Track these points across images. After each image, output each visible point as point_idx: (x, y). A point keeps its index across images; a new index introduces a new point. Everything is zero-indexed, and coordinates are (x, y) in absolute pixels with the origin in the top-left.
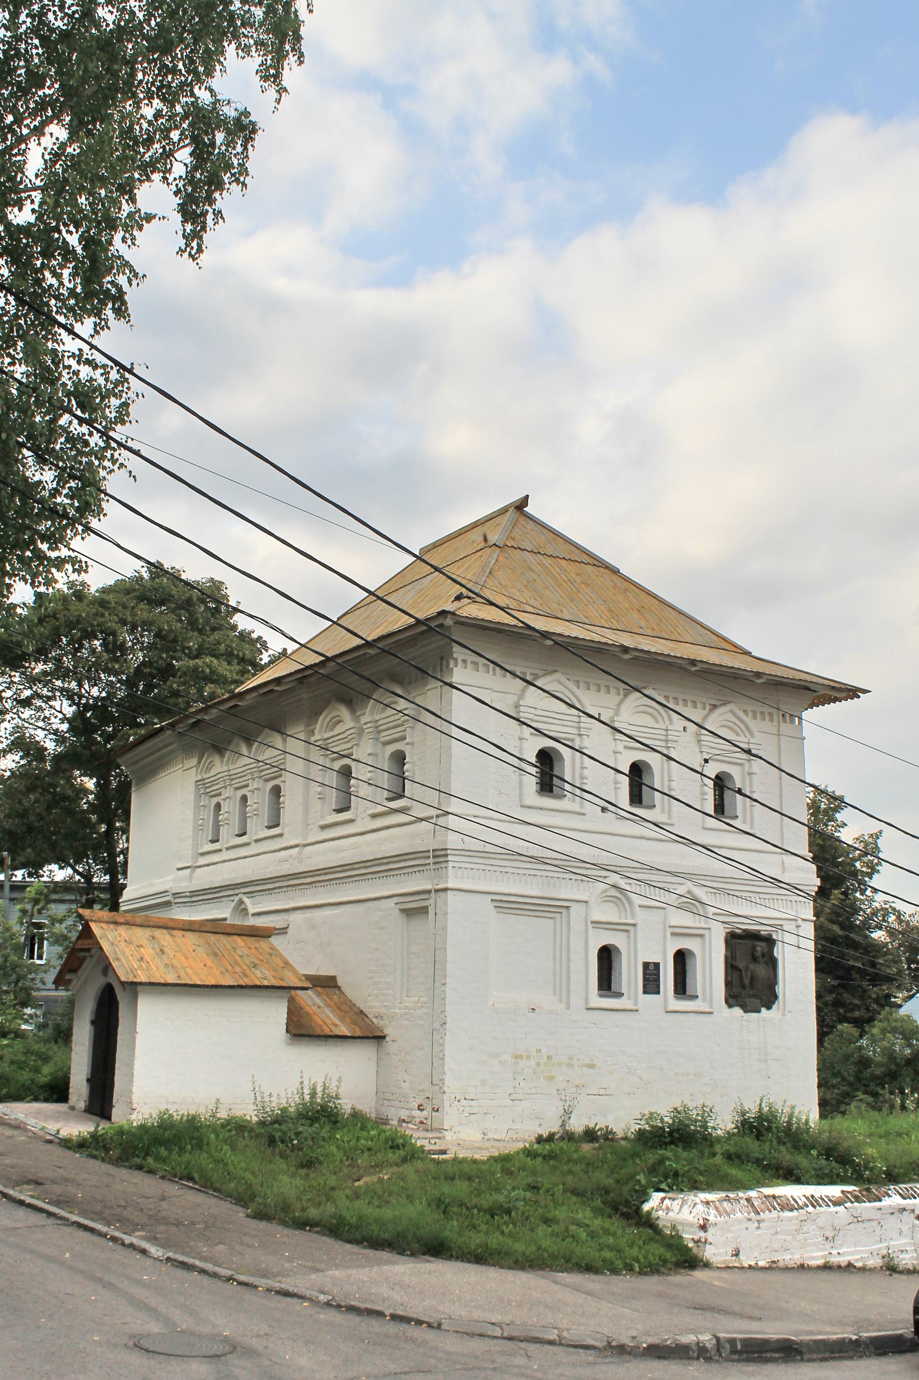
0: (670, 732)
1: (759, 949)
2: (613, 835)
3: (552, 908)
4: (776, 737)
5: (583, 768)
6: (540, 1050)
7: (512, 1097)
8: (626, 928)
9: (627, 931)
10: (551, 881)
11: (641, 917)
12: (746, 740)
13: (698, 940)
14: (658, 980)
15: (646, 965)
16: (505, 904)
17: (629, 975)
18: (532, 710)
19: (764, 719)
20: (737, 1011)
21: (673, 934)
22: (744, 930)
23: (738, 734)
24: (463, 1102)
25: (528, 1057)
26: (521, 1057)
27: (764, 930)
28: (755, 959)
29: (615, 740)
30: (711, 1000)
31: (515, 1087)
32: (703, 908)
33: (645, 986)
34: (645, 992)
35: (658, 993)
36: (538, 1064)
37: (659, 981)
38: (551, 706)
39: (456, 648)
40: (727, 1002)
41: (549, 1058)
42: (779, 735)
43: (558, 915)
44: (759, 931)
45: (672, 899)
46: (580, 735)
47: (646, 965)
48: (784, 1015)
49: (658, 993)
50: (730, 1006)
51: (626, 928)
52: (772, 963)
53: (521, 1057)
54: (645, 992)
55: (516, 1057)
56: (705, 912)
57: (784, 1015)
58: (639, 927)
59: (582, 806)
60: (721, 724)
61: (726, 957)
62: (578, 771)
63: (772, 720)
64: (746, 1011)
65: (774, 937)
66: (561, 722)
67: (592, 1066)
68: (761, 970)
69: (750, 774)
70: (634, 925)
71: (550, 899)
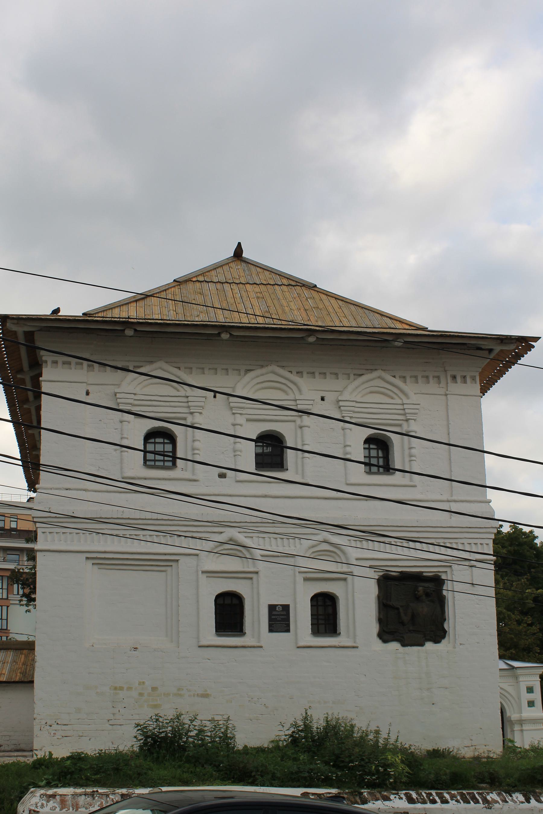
0: (190, 399)
1: (420, 589)
2: (245, 496)
3: (165, 563)
4: (444, 398)
5: (410, 448)
6: (144, 683)
7: (111, 722)
8: (248, 576)
9: (251, 579)
10: (63, 537)
11: (261, 566)
12: (400, 402)
13: (341, 583)
14: (288, 619)
15: (272, 608)
16: (101, 561)
17: (255, 616)
18: (132, 396)
19: (465, 382)
20: (395, 646)
21: (306, 579)
22: (401, 572)
23: (392, 398)
24: (55, 727)
25: (130, 689)
26: (121, 688)
27: (428, 571)
28: (417, 598)
29: (234, 414)
30: (355, 636)
31: (114, 714)
32: (248, 551)
33: (270, 626)
34: (271, 630)
35: (288, 631)
36: (141, 694)
37: (289, 621)
38: (151, 392)
39: (42, 353)
40: (444, 637)
41: (154, 689)
42: (446, 395)
43: (169, 569)
44: (423, 572)
45: (208, 546)
46: (192, 413)
47: (272, 608)
48: (454, 647)
49: (288, 631)
50: (385, 641)
51: (248, 576)
52: (441, 601)
53: (121, 688)
54: (271, 630)
55: (116, 688)
56: (251, 554)
57: (454, 647)
58: (261, 574)
59: (411, 480)
60: (368, 390)
61: (379, 597)
62: (407, 452)
63: (439, 383)
64: (403, 645)
65: (443, 577)
66: (168, 404)
67: (205, 696)
68: (424, 609)
69: (301, 427)
70: (257, 573)
71: (165, 554)
